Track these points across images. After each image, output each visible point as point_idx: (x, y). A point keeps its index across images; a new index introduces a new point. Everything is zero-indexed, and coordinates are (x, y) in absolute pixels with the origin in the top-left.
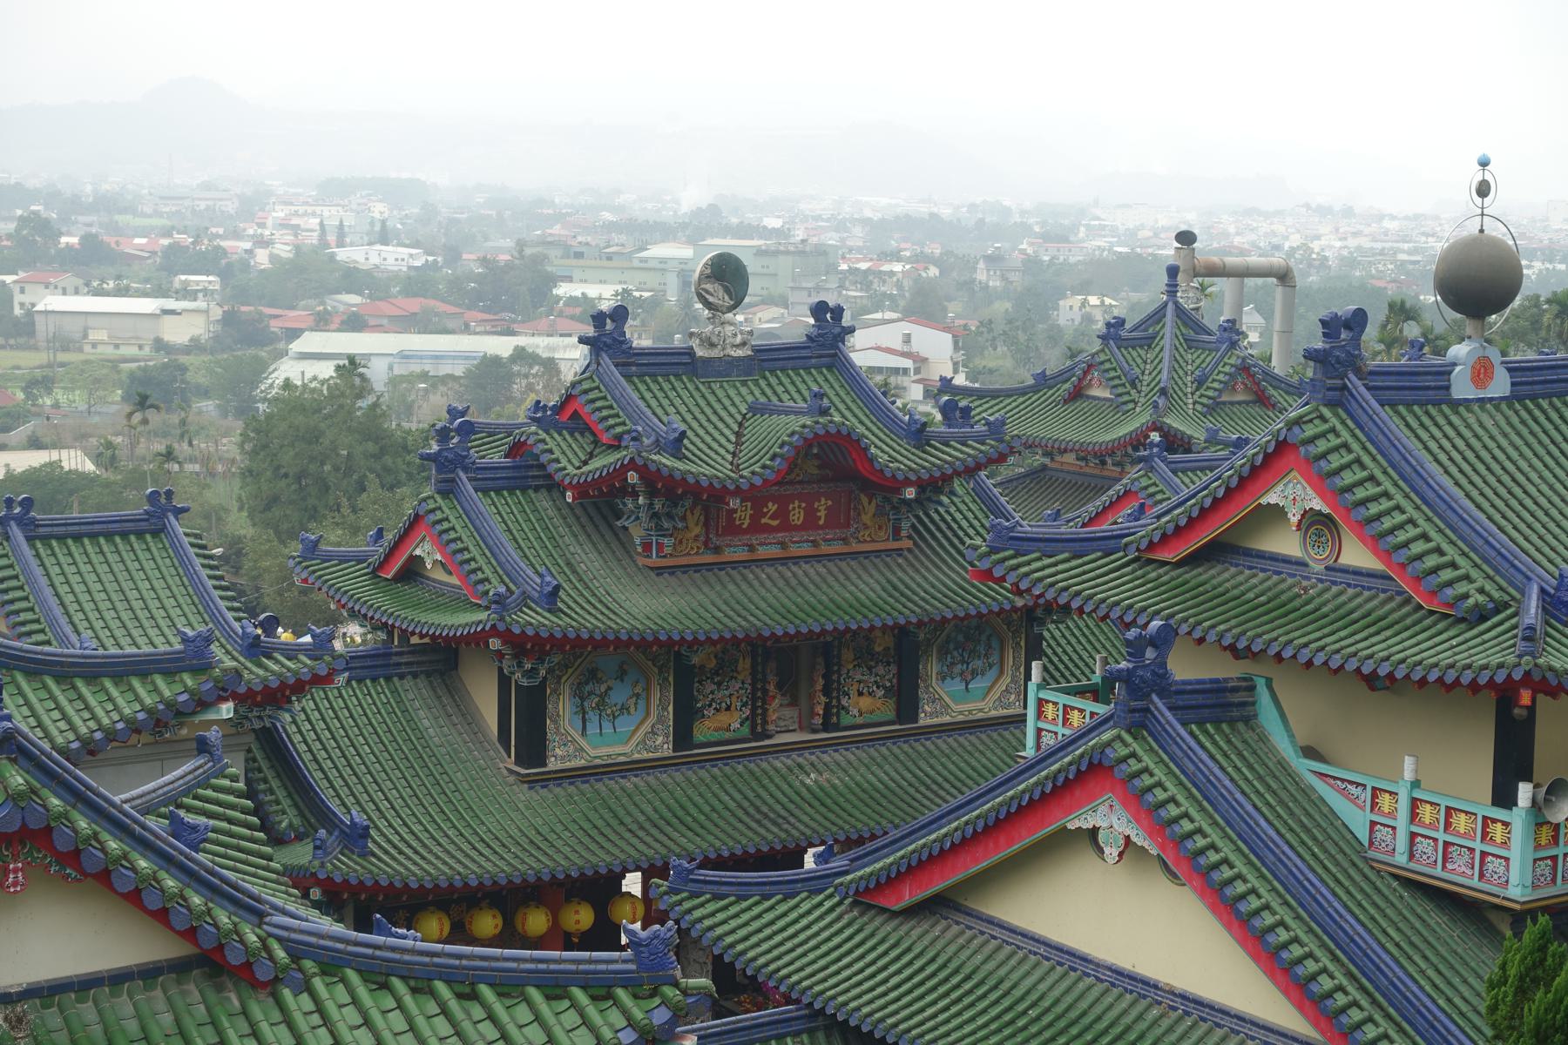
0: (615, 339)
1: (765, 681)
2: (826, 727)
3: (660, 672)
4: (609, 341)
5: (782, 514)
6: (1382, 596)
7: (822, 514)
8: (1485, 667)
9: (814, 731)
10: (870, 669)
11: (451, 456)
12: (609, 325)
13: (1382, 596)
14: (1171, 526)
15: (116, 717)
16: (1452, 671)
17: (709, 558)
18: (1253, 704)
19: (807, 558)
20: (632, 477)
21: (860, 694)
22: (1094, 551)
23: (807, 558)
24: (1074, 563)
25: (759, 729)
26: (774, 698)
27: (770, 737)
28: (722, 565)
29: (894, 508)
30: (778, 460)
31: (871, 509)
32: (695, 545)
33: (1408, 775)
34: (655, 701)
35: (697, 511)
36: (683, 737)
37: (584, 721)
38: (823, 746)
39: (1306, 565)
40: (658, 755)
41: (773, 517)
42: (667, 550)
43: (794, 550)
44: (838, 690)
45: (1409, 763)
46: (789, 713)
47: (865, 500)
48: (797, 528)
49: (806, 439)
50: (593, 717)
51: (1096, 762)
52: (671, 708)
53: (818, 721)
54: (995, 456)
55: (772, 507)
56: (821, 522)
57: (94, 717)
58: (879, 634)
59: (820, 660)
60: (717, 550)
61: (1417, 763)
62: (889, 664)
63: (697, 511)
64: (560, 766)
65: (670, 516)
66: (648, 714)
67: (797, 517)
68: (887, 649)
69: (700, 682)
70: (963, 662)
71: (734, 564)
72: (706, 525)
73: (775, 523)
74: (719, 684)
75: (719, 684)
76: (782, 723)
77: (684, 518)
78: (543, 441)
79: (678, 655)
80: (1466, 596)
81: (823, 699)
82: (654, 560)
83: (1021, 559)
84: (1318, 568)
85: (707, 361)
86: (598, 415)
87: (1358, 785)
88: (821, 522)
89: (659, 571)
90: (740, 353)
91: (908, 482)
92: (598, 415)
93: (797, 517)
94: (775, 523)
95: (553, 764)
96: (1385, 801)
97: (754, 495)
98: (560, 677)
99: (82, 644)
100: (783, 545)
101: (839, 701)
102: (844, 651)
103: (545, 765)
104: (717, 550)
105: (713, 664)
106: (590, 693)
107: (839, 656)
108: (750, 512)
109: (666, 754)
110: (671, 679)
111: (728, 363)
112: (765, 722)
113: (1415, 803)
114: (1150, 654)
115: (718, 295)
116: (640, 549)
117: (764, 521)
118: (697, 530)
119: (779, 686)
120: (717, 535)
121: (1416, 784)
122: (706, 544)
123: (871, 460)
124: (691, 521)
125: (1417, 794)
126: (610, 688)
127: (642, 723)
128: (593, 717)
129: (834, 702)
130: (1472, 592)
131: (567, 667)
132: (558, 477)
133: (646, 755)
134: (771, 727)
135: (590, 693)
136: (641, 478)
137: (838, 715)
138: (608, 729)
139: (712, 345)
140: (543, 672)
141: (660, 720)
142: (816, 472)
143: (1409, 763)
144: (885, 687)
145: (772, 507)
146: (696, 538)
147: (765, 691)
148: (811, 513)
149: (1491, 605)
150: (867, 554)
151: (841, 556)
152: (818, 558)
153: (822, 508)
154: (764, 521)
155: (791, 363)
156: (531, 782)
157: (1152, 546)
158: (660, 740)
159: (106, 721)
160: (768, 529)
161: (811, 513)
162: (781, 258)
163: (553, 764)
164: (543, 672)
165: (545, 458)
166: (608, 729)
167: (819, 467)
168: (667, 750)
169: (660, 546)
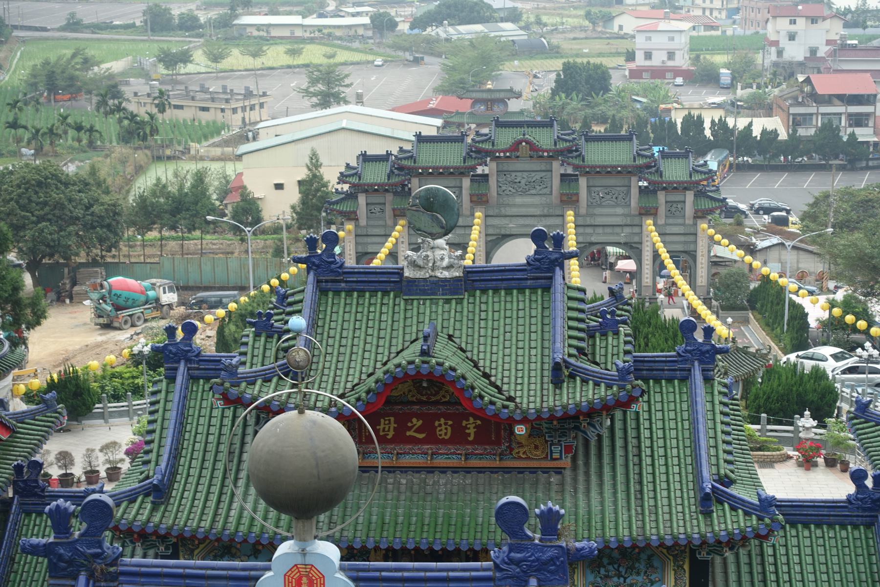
4: (317, 262)
5: (428, 428)
7: (472, 431)
11: (174, 350)
15: (723, 526)
23: (455, 470)
41: (418, 431)
48: (444, 442)
55: (417, 423)
56: (471, 438)
57: (657, 528)
70: (619, 576)
85: (412, 281)
88: (471, 438)
90: (446, 274)
99: (868, 75)
108: (393, 425)
110: (686, 567)
111: (433, 283)
117: (408, 433)
139: (420, 268)
145: (417, 423)
150: (521, 470)
151: (494, 470)
152: (468, 470)
155: (504, 284)
159: (730, 527)
160: (413, 441)
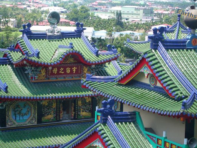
0: (28, 31)
1: (59, 108)
2: (75, 119)
3: (34, 106)
5: (65, 70)
6: (164, 93)
7: (74, 71)
8: (174, 112)
9: (72, 120)
10: (85, 106)
12: (27, 27)
13: (164, 93)
14: (123, 76)
16: (171, 112)
17: (47, 80)
18: (135, 118)
19: (70, 81)
20: (25, 62)
21: (83, 111)
22: (109, 81)
24: (105, 84)
25: (58, 119)
26: (62, 112)
27: (61, 121)
28: (50, 82)
29: (92, 70)
30: (61, 59)
31: (86, 70)
32: (43, 77)
33: (164, 136)
34: (33, 111)
35: (44, 70)
36: (39, 121)
37: (16, 117)
38: (74, 123)
39: (150, 86)
40: (34, 124)
41: (62, 71)
42: (36, 79)
43: (67, 79)
44: (77, 110)
45: (164, 133)
46: (66, 115)
47: (85, 68)
49: (67, 54)
50: (18, 116)
51: (95, 131)
52: (36, 114)
53: (73, 117)
54: (114, 58)
55: (62, 69)
56: (74, 73)
58: (87, 98)
59: (73, 104)
60: (49, 79)
61: (166, 132)
62: (90, 105)
63: (44, 70)
64: (10, 127)
65: (36, 71)
66: (31, 116)
67: (68, 71)
68: (89, 101)
69: (44, 108)
71: (53, 82)
72: (46, 73)
73: (63, 73)
74: (48, 109)
75: (48, 109)
76: (64, 118)
77: (40, 71)
78: (10, 54)
79: (38, 103)
80: (177, 94)
81: (74, 113)
82: (33, 81)
83: (93, 83)
84: (152, 87)
86: (22, 48)
87: (155, 138)
88: (74, 73)
89: (34, 83)
91: (93, 64)
92: (22, 48)
93: (68, 71)
94: (63, 73)
95: (8, 126)
96: (160, 141)
97: (54, 66)
98: (9, 107)
100: (65, 78)
101: (77, 113)
102: (79, 102)
103: (6, 127)
104: (49, 79)
105: (47, 104)
106: (17, 110)
107: (78, 103)
108: (56, 70)
109: (35, 124)
110: (36, 108)
112: (59, 117)
113: (165, 142)
114: (108, 106)
115: (54, 21)
116: (30, 78)
117: (60, 72)
118: (44, 74)
119: (64, 110)
120: (49, 75)
121: (166, 138)
122: (46, 77)
123: (84, 59)
124: (42, 72)
125: (166, 140)
126: (22, 109)
127: (30, 117)
128: (18, 116)
129: (76, 113)
130: (179, 93)
131: (11, 105)
132: (12, 62)
133: (30, 124)
134: (61, 119)
135: (17, 110)
136: (27, 62)
137: (77, 116)
138: (21, 118)
140: (4, 106)
141: (34, 117)
142: (73, 61)
143: (164, 133)
144: (89, 110)
145: (62, 69)
146: (44, 75)
147: (60, 111)
148: (72, 71)
149: (184, 96)
153: (74, 69)
154: (60, 72)
156: (3, 130)
157: (119, 81)
158: (34, 121)
161: (72, 71)
162: (141, 10)
163: (8, 126)
164: (4, 106)
165: (10, 57)
166: (21, 118)
167: (74, 60)
168: (36, 123)
169: (35, 78)
